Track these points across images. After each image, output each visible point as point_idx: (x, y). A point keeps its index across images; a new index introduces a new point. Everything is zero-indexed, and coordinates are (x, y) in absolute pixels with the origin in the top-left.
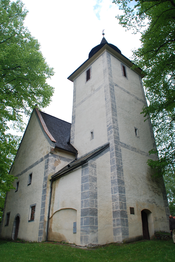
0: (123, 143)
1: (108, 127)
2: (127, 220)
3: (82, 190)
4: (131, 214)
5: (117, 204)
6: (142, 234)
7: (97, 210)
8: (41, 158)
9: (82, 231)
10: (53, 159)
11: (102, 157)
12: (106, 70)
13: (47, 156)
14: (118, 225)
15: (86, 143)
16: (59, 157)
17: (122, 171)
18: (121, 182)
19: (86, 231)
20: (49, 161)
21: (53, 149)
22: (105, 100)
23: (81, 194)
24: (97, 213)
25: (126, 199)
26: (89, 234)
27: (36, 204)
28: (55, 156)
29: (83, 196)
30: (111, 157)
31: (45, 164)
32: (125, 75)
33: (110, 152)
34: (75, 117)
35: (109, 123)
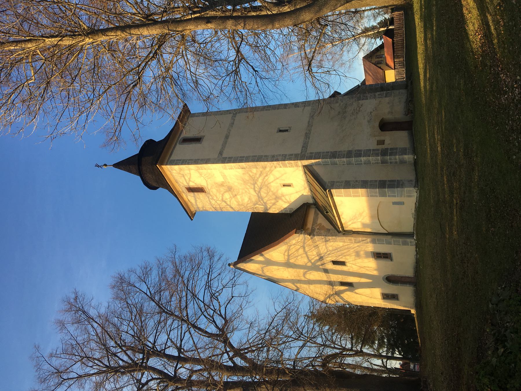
1: (282, 166)
2: (391, 149)
4: (384, 144)
5: (373, 159)
7: (380, 181)
9: (401, 196)
10: (317, 232)
16: (314, 225)
17: (336, 152)
18: (349, 154)
32: (197, 140)
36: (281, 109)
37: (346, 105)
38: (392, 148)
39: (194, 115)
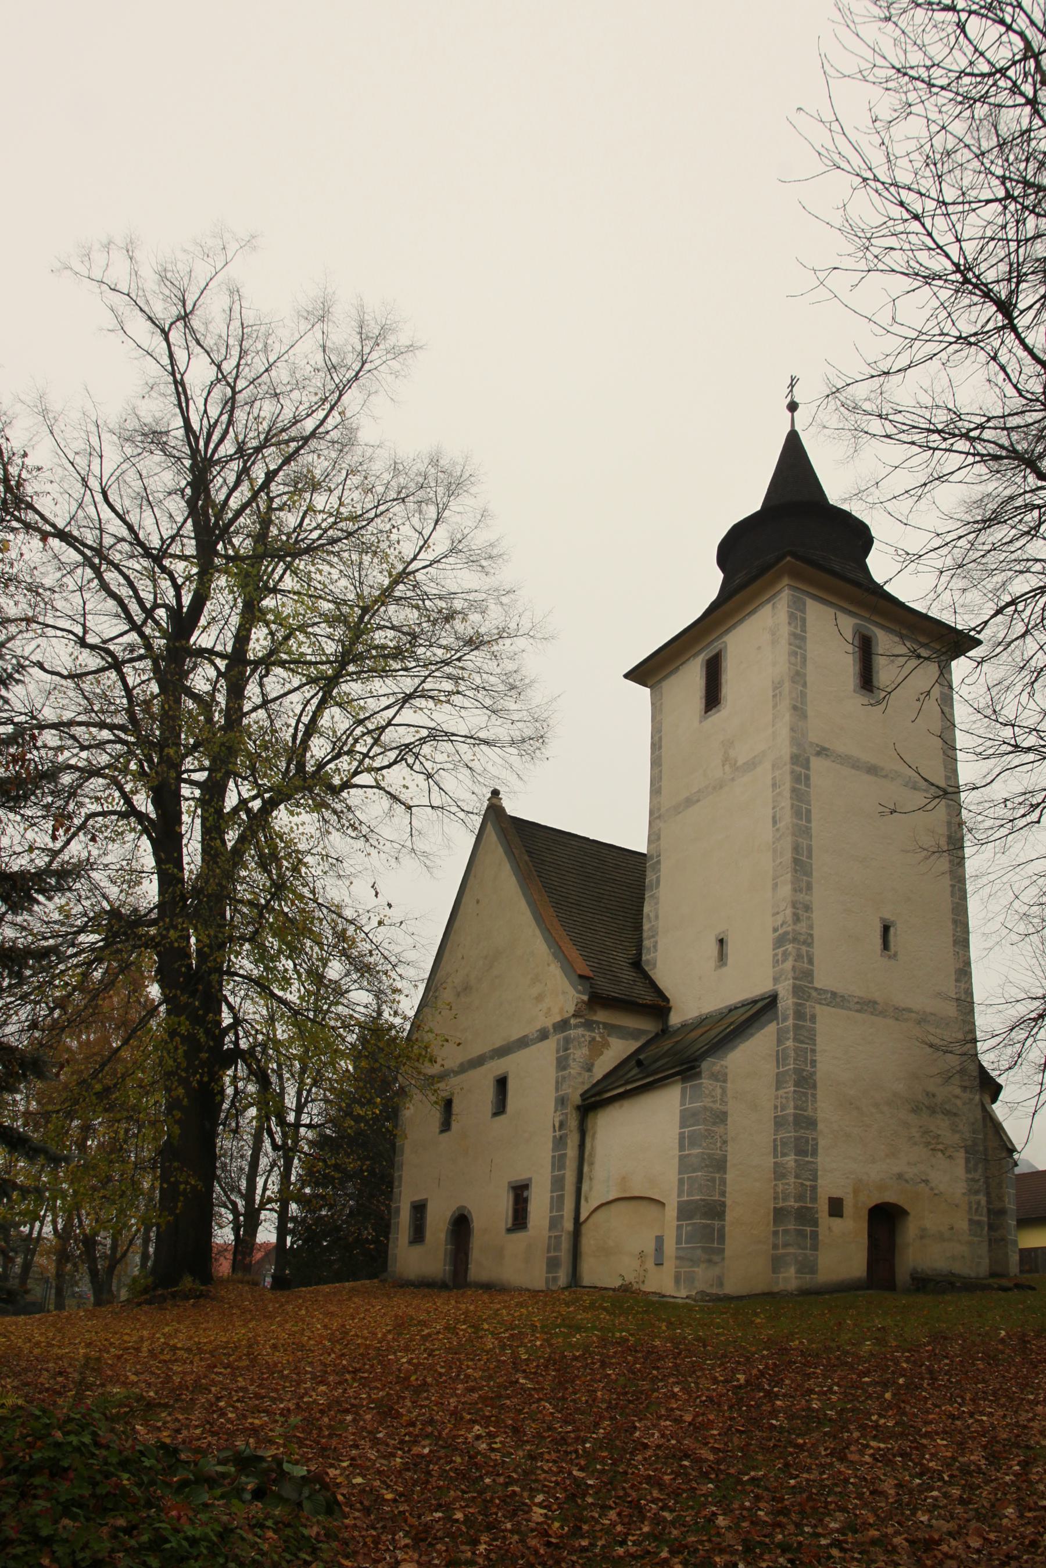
0: (825, 991)
2: (815, 1235)
3: (682, 1147)
6: (865, 1274)
7: (723, 1204)
8: (539, 1027)
9: (677, 1258)
10: (583, 1036)
11: (747, 1044)
12: (781, 683)
13: (563, 1025)
14: (786, 1245)
15: (700, 978)
16: (604, 1028)
17: (814, 1087)
19: (692, 1260)
20: (571, 1046)
21: (583, 1002)
22: (770, 821)
23: (677, 1160)
24: (724, 1212)
25: (819, 1173)
26: (698, 1266)
27: (530, 1179)
28: (589, 1025)
29: (684, 1164)
30: (779, 1042)
31: (558, 1051)
33: (778, 1024)
34: (659, 862)
35: (780, 919)
36: (955, 930)
37: (955, 1114)
38: (817, 1235)
39: (944, 671)
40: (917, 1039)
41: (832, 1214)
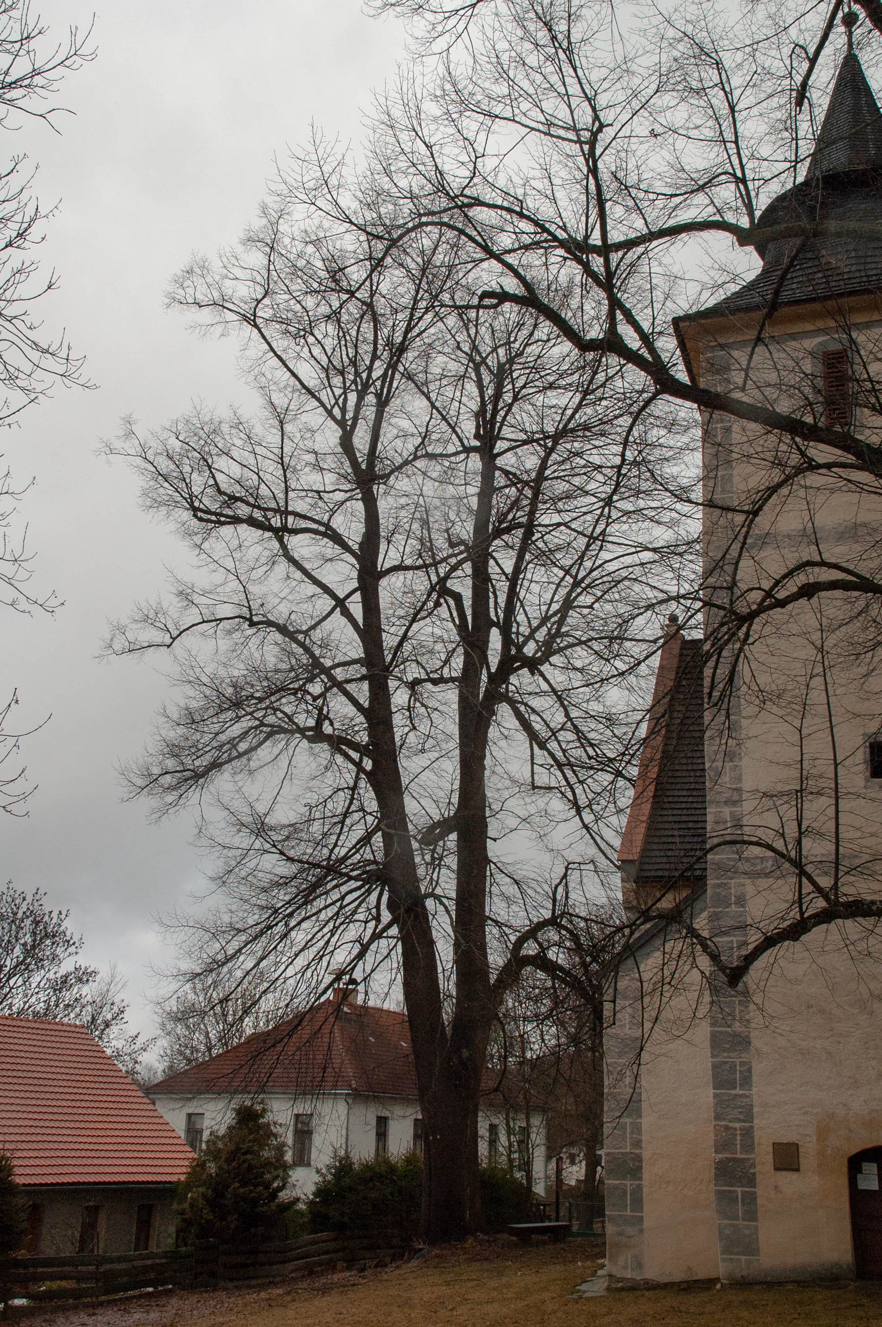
2: (750, 1199)
4: (777, 1169)
7: (638, 1158)
24: (640, 1168)
25: (755, 1110)
40: (113, 976)
41: (779, 1167)
